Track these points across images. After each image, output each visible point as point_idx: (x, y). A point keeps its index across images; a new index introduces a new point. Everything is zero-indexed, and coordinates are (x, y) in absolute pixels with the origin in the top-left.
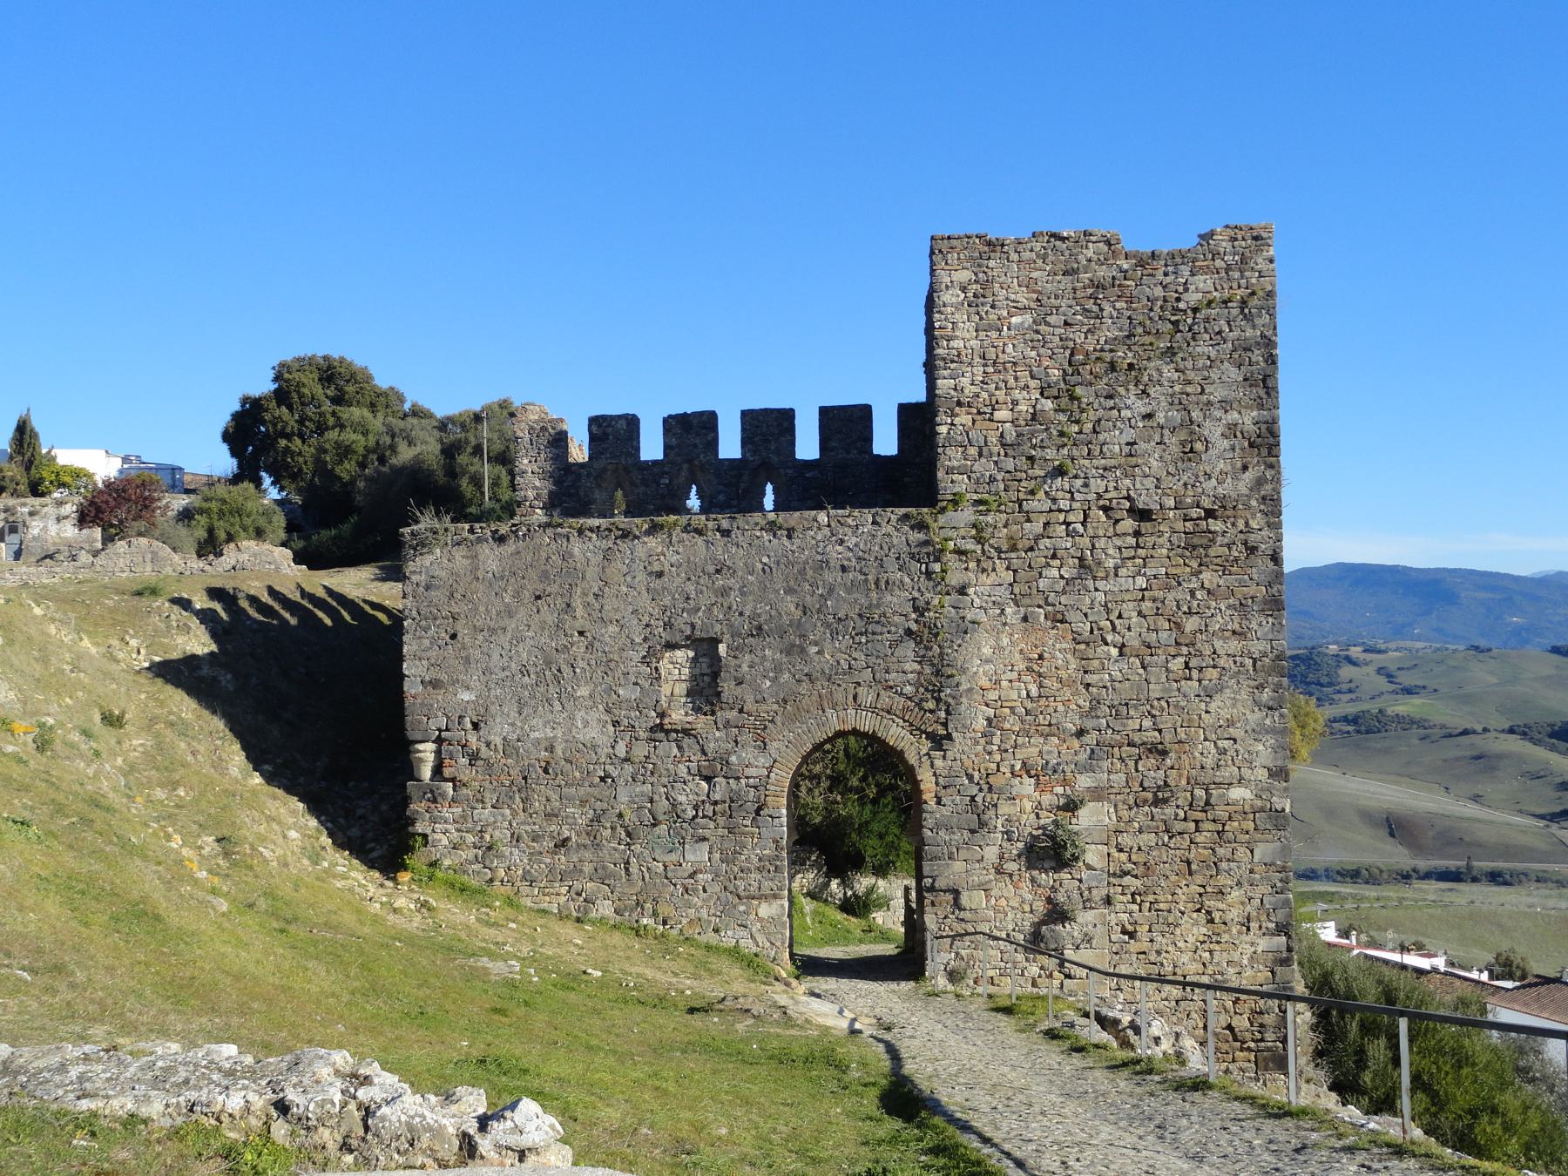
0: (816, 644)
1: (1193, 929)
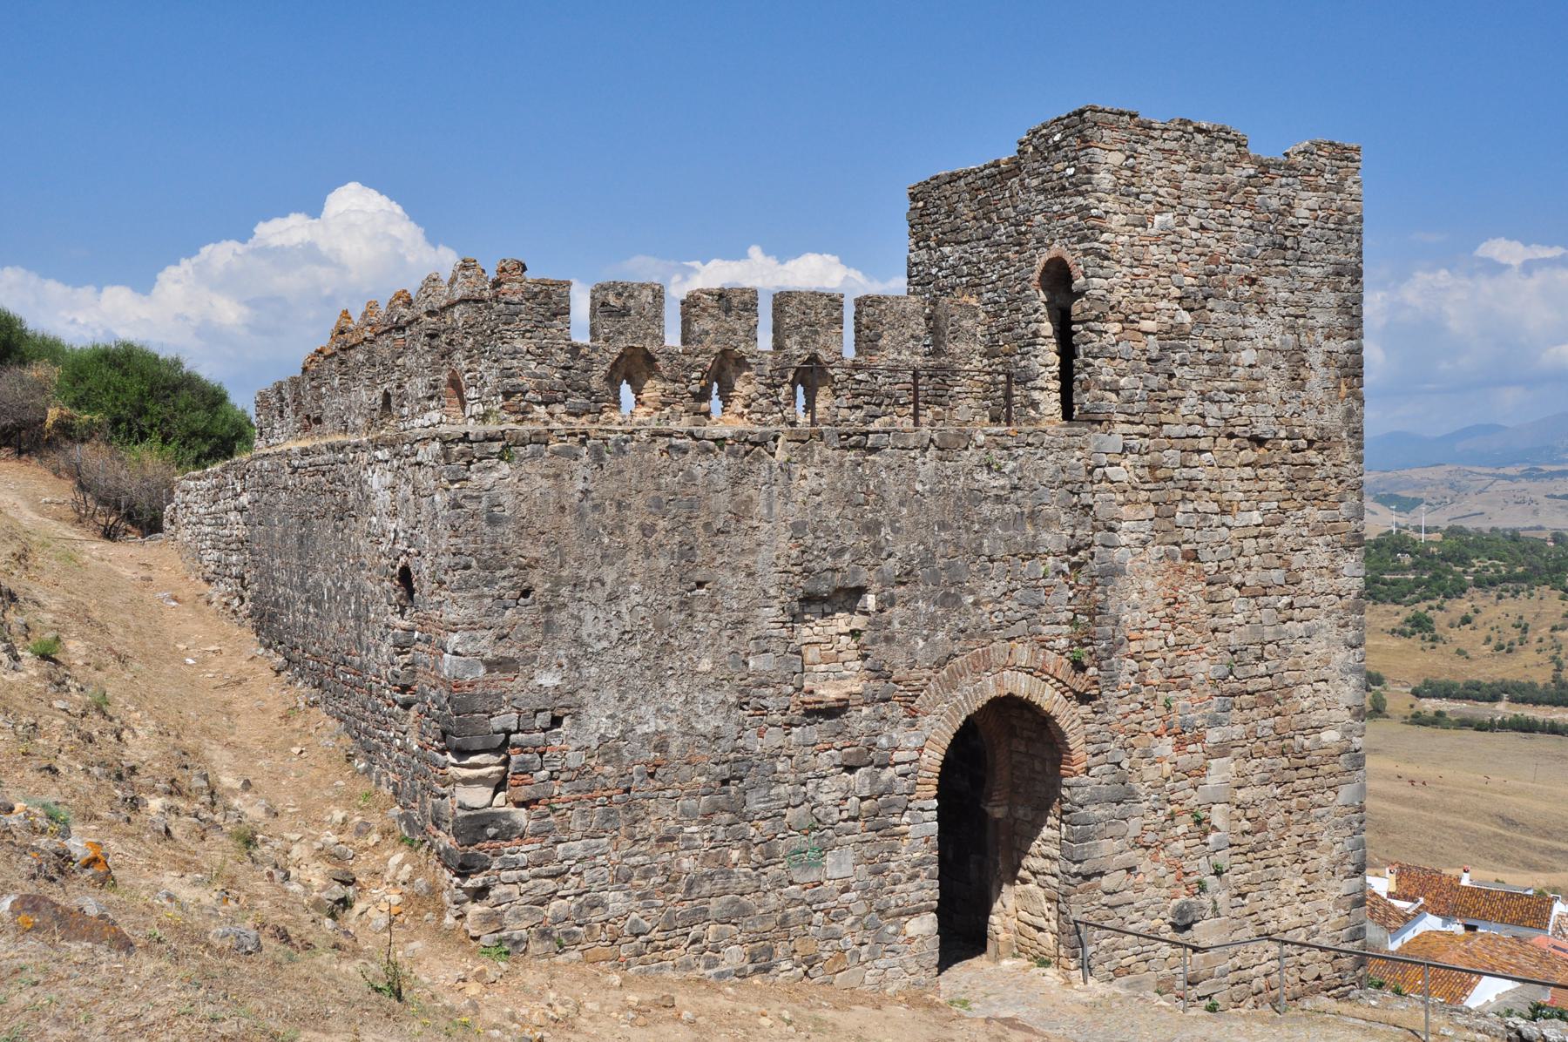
0: (972, 592)
1: (1293, 882)
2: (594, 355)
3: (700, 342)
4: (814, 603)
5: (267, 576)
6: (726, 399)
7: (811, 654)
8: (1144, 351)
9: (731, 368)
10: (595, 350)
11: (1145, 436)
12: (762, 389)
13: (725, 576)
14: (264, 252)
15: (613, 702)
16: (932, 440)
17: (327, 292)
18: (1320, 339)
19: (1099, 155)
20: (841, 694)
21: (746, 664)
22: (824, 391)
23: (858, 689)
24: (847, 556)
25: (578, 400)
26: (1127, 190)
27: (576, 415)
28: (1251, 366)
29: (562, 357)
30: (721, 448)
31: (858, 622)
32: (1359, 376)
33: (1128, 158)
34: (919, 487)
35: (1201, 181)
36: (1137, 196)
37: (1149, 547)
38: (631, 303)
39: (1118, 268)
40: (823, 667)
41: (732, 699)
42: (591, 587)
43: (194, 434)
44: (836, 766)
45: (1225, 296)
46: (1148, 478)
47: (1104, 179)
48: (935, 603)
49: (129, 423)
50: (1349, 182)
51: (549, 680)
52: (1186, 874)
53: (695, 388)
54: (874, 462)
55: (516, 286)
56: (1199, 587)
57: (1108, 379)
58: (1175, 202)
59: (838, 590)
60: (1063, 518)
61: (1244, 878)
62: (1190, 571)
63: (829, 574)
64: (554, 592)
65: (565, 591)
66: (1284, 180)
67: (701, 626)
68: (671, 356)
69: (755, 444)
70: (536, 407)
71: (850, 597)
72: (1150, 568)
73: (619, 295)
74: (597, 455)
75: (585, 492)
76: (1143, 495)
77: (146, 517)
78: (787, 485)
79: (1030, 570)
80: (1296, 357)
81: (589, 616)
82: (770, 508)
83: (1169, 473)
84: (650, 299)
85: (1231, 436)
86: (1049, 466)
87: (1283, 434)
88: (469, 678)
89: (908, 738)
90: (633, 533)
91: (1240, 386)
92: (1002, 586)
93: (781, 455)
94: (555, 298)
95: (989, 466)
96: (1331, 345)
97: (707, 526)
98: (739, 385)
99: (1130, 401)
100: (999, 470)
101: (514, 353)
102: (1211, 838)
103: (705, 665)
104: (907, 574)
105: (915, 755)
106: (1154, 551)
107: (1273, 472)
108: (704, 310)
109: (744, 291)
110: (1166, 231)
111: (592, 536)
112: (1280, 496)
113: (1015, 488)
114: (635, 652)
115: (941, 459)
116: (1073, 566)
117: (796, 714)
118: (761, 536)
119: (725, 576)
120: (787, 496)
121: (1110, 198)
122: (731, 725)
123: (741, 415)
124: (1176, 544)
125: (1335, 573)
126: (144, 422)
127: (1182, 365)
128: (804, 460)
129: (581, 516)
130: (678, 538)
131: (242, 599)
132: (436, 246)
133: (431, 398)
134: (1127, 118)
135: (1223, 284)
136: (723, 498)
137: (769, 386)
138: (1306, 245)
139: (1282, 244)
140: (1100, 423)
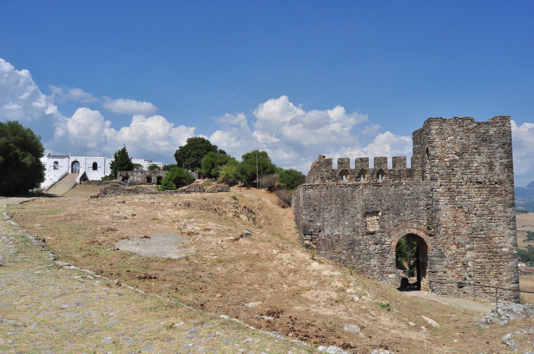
4: (367, 214)
6: (364, 177)
7: (369, 223)
13: (350, 208)
19: (432, 127)
23: (378, 230)
25: (334, 179)
26: (440, 133)
29: (331, 172)
31: (378, 218)
32: (512, 167)
35: (461, 129)
47: (434, 132)
51: (319, 224)
59: (374, 212)
65: (321, 210)
68: (351, 170)
71: (376, 213)
76: (446, 194)
85: (471, 182)
86: (421, 189)
87: (487, 181)
90: (333, 201)
92: (410, 212)
93: (361, 187)
96: (502, 161)
99: (442, 175)
101: (322, 171)
102: (468, 269)
103: (347, 223)
106: (449, 206)
107: (484, 189)
110: (451, 140)
111: (326, 201)
113: (413, 193)
114: (334, 220)
117: (365, 234)
119: (350, 208)
120: (362, 195)
125: (506, 212)
127: (456, 167)
129: (324, 198)
136: (350, 195)
138: (493, 139)
139: (485, 140)
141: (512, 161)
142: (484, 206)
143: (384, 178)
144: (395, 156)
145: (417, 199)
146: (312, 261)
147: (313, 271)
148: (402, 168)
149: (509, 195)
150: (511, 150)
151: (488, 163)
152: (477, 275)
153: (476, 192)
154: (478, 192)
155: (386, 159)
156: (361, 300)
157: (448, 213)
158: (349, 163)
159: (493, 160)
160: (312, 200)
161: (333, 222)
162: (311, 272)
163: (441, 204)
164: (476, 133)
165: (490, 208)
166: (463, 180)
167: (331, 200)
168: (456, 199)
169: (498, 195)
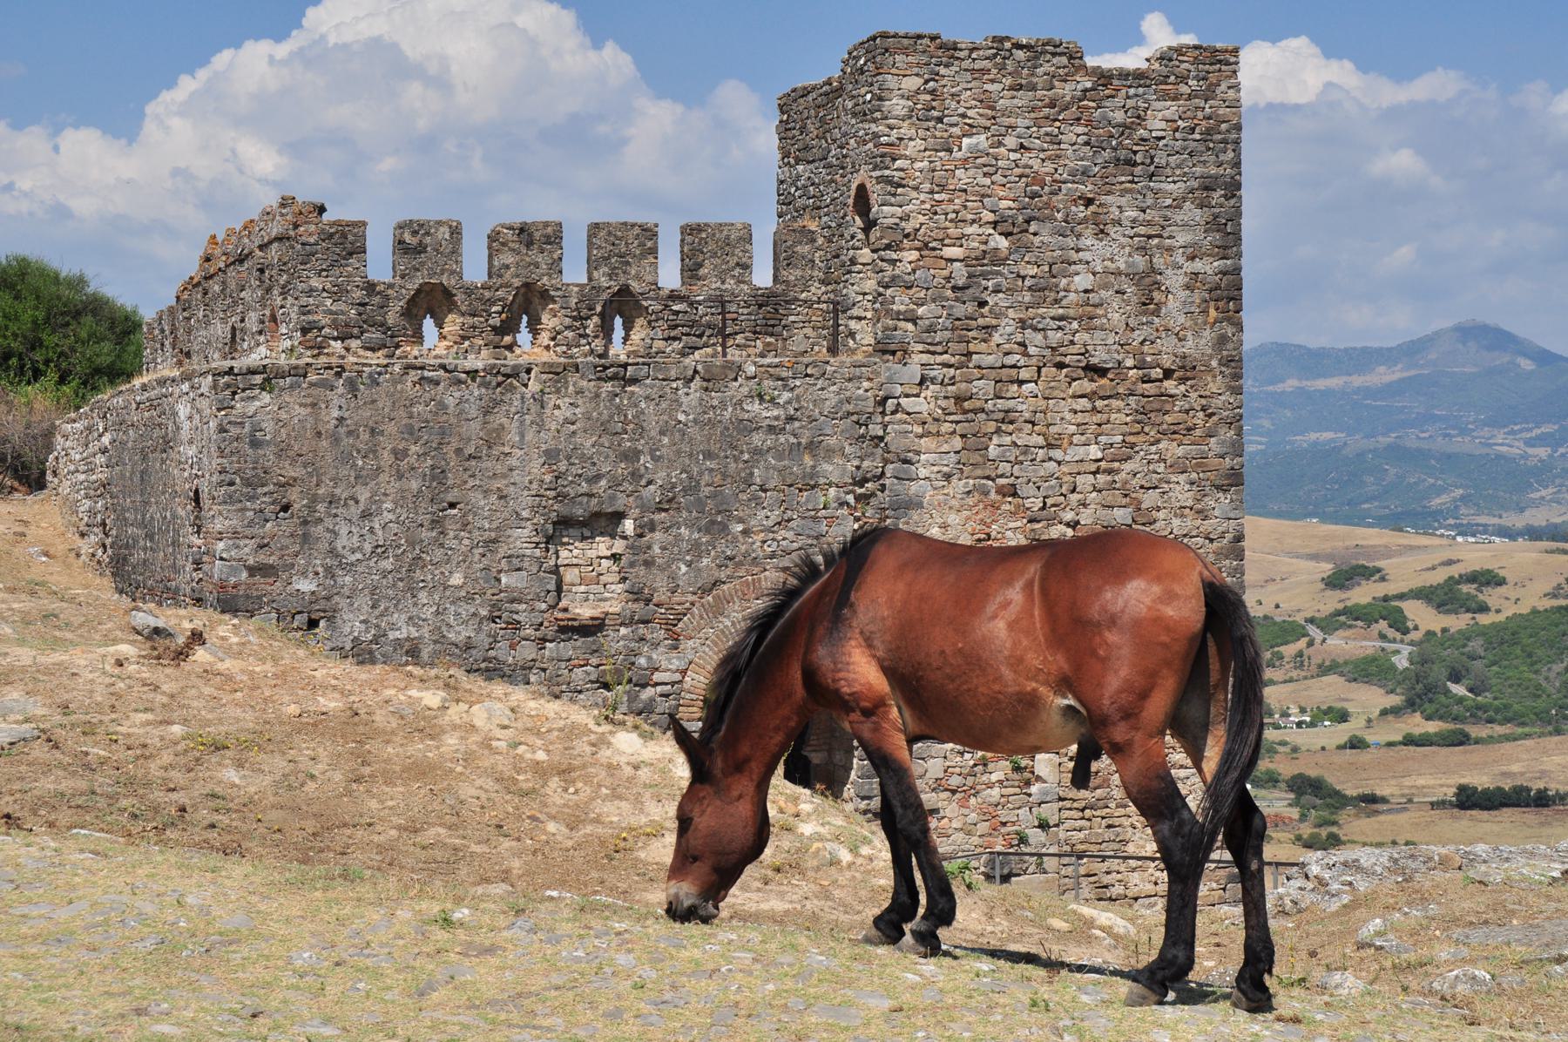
0: (741, 521)
2: (390, 292)
3: (500, 276)
4: (562, 527)
5: (122, 521)
6: (534, 331)
7: (570, 576)
8: (948, 279)
9: (536, 300)
10: (391, 286)
11: (950, 366)
12: (568, 321)
13: (477, 498)
14: (317, 57)
15: (366, 608)
16: (696, 372)
17: (422, 124)
18: (1181, 260)
19: (891, 82)
20: (596, 613)
21: (499, 580)
22: (640, 322)
23: (617, 609)
24: (603, 483)
25: (374, 335)
26: (928, 113)
27: (373, 350)
28: (1086, 291)
29: (358, 294)
30: (474, 380)
31: (619, 546)
32: (1237, 299)
33: (926, 82)
34: (682, 417)
35: (1023, 99)
36: (940, 120)
37: (954, 480)
38: (428, 240)
39: (914, 194)
40: (583, 588)
41: (484, 612)
42: (345, 504)
43: (98, 371)
44: (592, 682)
45: (1052, 219)
46: (953, 409)
47: (897, 106)
48: (700, 530)
49: (21, 358)
50: (1223, 87)
51: (306, 586)
52: (1004, 824)
53: (495, 321)
54: (633, 393)
55: (312, 228)
56: (1019, 524)
57: (903, 308)
58: (988, 123)
59: (597, 515)
60: (848, 450)
61: (1081, 835)
62: (1007, 507)
63: (585, 499)
64: (311, 508)
65: (321, 507)
66: (1132, 91)
67: (454, 544)
68: (469, 291)
69: (508, 376)
70: (332, 343)
71: (605, 522)
72: (954, 502)
73: (415, 233)
74: (352, 386)
75: (341, 420)
76: (946, 427)
77: (35, 472)
78: (540, 415)
79: (807, 501)
80: (1148, 281)
81: (344, 531)
82: (522, 436)
83: (978, 404)
84: (447, 236)
85: (1060, 366)
86: (831, 396)
87: (1129, 362)
88: (233, 580)
89: (669, 660)
90: (386, 457)
91: (1071, 312)
92: (775, 515)
93: (534, 386)
94: (350, 237)
95: (761, 397)
96: (1198, 265)
97: (459, 451)
98: (545, 318)
99: (930, 329)
100: (772, 400)
101: (310, 292)
102: (1034, 789)
103: (457, 579)
104: (670, 501)
105: (678, 677)
106: (959, 485)
107: (1115, 403)
108: (503, 244)
109: (546, 224)
110: (977, 153)
111: (346, 458)
112: (1127, 429)
113: (790, 419)
114: (387, 564)
115: (706, 389)
116: (858, 498)
117: (550, 632)
118: (514, 462)
119: (477, 498)
120: (540, 426)
121: (905, 124)
122: (482, 636)
123: (547, 348)
124: (988, 478)
125: (1203, 514)
126: (38, 356)
127: (997, 291)
128: (558, 391)
129: (336, 440)
130: (429, 462)
131: (104, 546)
132: (597, 45)
133: (260, 333)
134: (926, 41)
135: (1047, 205)
136: (475, 426)
137: (574, 319)
138: (1160, 158)
139: (1129, 160)
140: (893, 353)
141: (1237, 271)
142: (1111, 486)
143: (637, 335)
144: (693, 220)
145: (812, 447)
146: (606, 728)
147: (636, 768)
148: (730, 284)
149: (1223, 430)
150: (1237, 213)
151: (1135, 277)
152: (1072, 819)
153: (1080, 418)
154: (1087, 418)
155: (649, 232)
156: (860, 861)
157: (953, 519)
158: (455, 252)
159: (1158, 261)
160: (269, 452)
161: (385, 574)
162: (628, 770)
163: (923, 472)
164: (1089, 123)
165: (1140, 495)
166: (1026, 354)
167: (373, 451)
168: (993, 451)
169: (1172, 433)
